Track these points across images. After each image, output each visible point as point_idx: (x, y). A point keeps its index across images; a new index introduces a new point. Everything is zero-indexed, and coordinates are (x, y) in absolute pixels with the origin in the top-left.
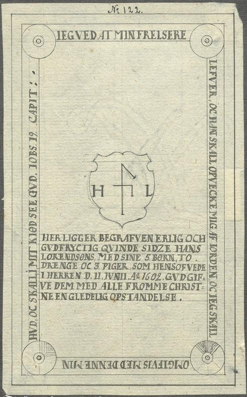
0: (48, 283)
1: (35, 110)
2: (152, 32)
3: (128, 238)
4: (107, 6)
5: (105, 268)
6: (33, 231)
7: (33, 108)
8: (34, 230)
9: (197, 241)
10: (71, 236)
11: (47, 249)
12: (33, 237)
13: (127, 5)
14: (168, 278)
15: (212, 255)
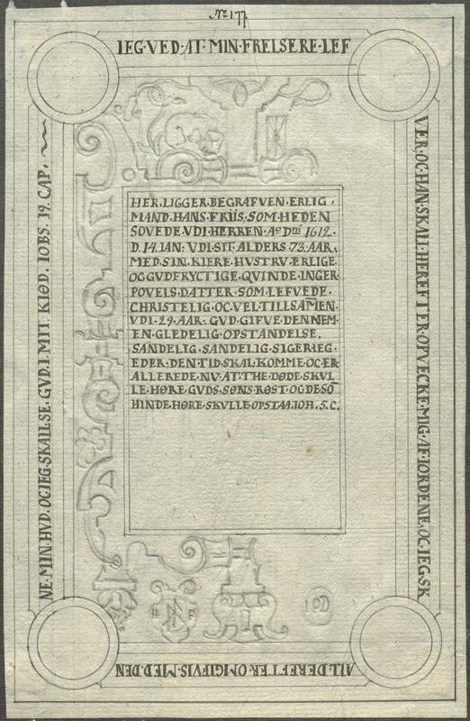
6: (44, 292)
8: (46, 290)
15: (423, 478)
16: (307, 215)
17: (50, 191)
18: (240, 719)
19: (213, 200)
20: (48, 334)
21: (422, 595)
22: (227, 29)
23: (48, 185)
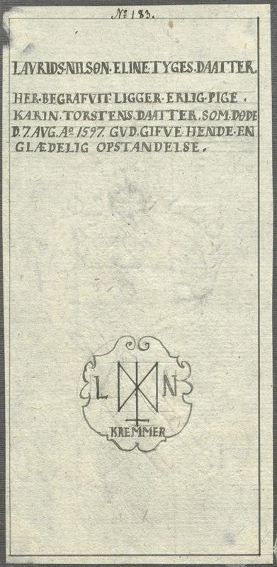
0: (177, 128)
2: (116, 63)
3: (217, 67)
4: (113, 10)
5: (213, 99)
10: (127, 95)
14: (113, 134)
16: (161, 144)
18: (114, 565)
19: (212, 95)
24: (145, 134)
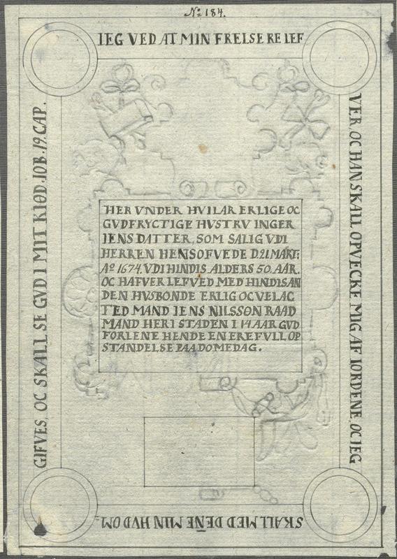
1: (43, 116)
4: (186, 8)
7: (40, 453)
9: (351, 277)
11: (44, 297)
12: (39, 212)
13: (210, 7)
16: (127, 222)
17: (45, 127)
20: (45, 242)
21: (187, 240)
22: (198, 25)
23: (42, 121)
24: (44, 302)
